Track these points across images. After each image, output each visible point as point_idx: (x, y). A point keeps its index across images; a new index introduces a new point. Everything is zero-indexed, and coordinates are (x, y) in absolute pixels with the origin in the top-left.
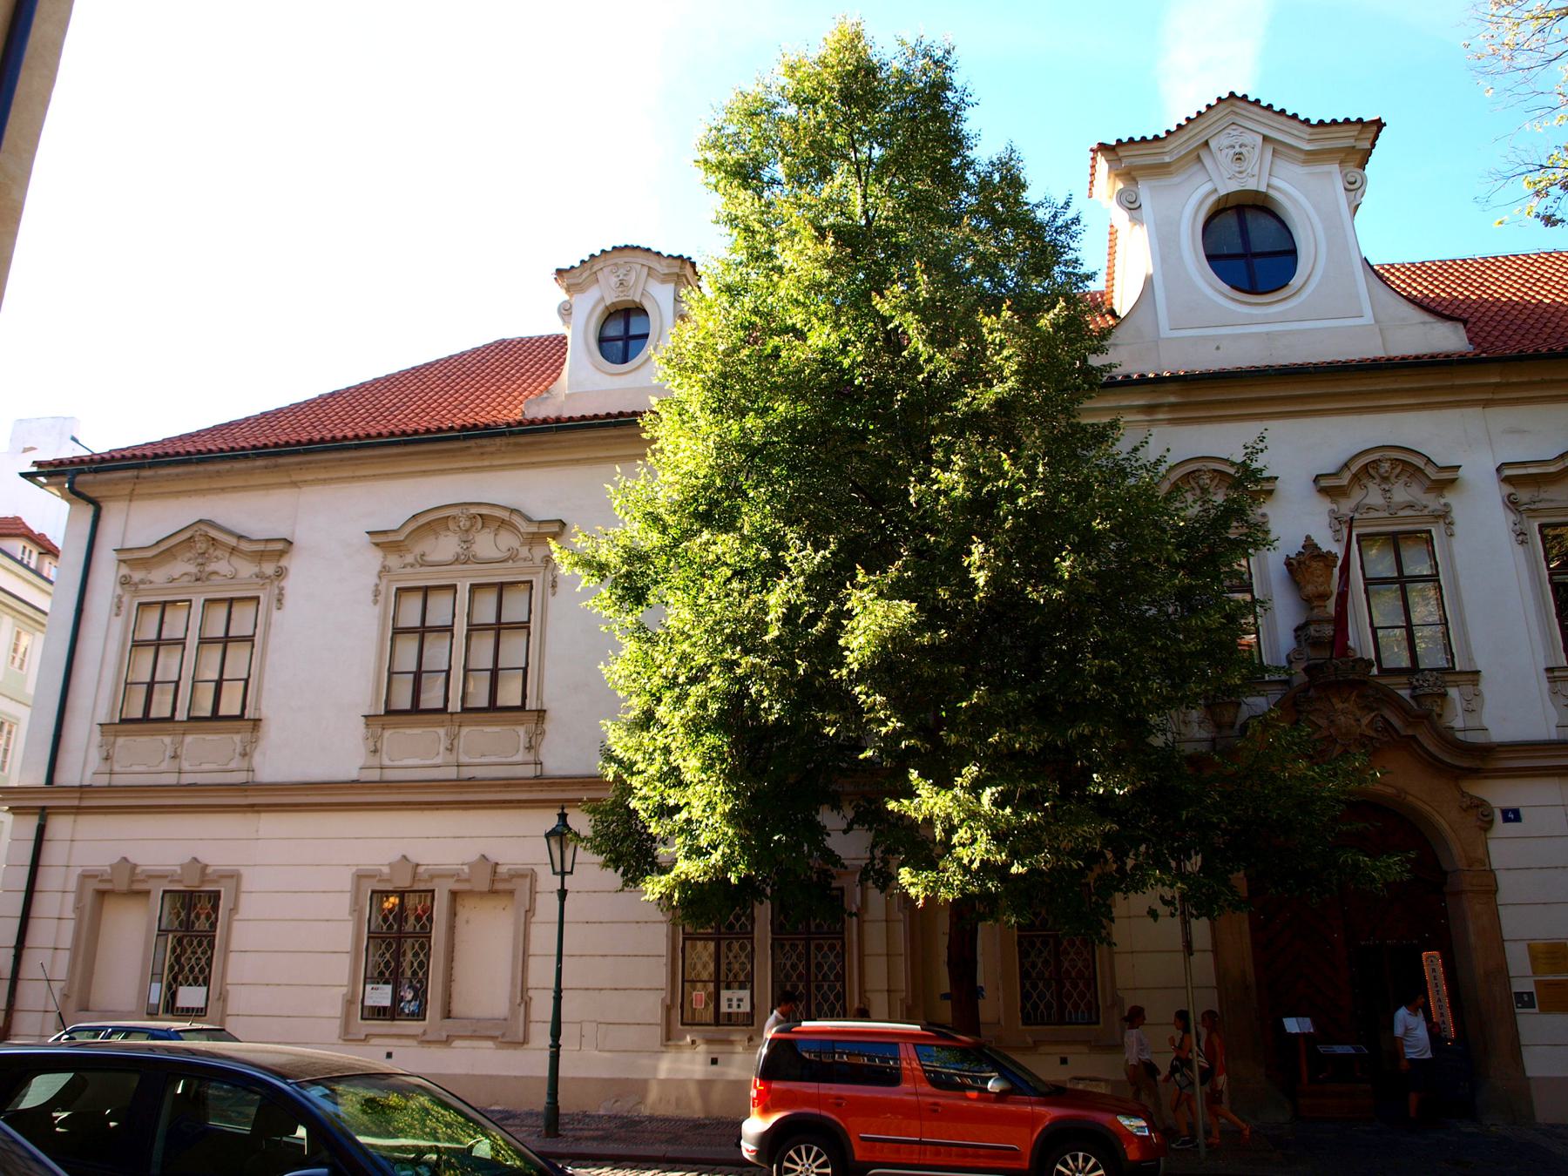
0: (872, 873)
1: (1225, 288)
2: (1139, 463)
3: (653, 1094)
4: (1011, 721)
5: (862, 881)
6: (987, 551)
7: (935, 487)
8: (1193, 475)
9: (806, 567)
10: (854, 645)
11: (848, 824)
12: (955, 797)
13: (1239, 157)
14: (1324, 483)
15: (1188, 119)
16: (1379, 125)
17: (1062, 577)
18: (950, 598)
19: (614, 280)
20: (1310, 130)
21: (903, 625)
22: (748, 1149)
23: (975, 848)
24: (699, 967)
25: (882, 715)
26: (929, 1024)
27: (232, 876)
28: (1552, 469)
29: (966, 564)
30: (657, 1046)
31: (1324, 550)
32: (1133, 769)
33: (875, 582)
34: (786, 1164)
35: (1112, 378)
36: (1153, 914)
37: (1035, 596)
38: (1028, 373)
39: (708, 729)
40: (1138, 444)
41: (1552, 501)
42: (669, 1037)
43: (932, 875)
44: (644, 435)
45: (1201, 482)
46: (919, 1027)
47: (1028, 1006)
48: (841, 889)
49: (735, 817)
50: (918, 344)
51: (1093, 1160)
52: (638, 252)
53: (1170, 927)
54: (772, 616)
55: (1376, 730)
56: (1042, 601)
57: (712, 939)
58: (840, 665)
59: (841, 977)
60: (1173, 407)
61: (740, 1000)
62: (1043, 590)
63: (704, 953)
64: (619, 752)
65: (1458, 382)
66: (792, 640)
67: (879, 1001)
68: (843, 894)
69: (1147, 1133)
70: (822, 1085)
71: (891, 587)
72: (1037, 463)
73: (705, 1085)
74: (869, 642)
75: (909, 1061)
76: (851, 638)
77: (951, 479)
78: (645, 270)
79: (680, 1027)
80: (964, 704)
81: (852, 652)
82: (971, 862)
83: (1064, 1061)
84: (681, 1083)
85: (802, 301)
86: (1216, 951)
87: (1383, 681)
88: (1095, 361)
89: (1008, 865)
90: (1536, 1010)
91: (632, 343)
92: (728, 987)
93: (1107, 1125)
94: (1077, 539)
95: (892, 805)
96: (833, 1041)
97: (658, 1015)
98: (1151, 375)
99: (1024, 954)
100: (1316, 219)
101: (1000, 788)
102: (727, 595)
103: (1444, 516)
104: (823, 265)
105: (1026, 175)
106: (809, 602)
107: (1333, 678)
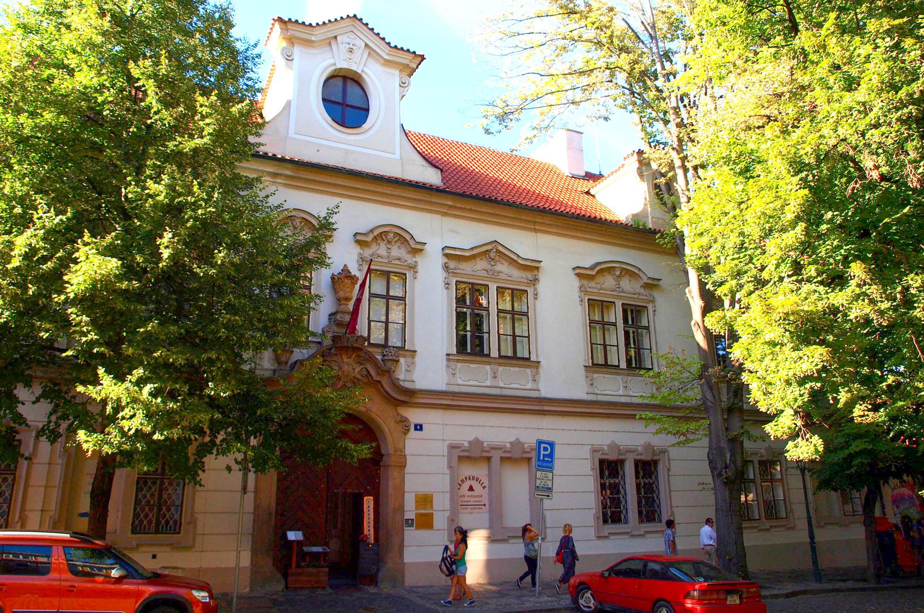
0: (47, 432)
1: (329, 119)
2: (267, 205)
4: (171, 343)
5: (37, 437)
6: (173, 238)
7: (147, 191)
9: (47, 224)
10: (73, 281)
11: (37, 398)
13: (351, 51)
14: (359, 238)
16: (423, 58)
17: (216, 262)
20: (390, 49)
21: (110, 274)
25: (85, 329)
26: (74, 533)
28: (467, 254)
29: (158, 243)
31: (353, 274)
32: (233, 382)
33: (95, 243)
35: (257, 152)
36: (229, 469)
37: (198, 270)
38: (218, 136)
40: (269, 194)
41: (463, 270)
43: (100, 437)
45: (294, 223)
46: (69, 535)
47: (137, 522)
48: (20, 441)
50: (152, 101)
53: (237, 475)
54: (16, 252)
55: (362, 376)
56: (202, 274)
58: (60, 292)
60: (287, 176)
62: (204, 268)
65: (434, 200)
66: (28, 271)
67: (34, 517)
69: (208, 600)
71: (106, 248)
72: (213, 191)
74: (85, 281)
75: (58, 557)
76: (74, 276)
77: (158, 190)
80: (142, 330)
81: (72, 285)
82: (130, 429)
83: (154, 557)
85: (79, 51)
86: (256, 492)
87: (370, 349)
88: (252, 139)
90: (414, 528)
93: (185, 596)
94: (229, 241)
95: (80, 388)
98: (279, 156)
99: (139, 489)
100: (382, 97)
101: (156, 385)
103: (413, 267)
104: (99, 33)
105: (235, 20)
106: (44, 248)
107: (346, 344)
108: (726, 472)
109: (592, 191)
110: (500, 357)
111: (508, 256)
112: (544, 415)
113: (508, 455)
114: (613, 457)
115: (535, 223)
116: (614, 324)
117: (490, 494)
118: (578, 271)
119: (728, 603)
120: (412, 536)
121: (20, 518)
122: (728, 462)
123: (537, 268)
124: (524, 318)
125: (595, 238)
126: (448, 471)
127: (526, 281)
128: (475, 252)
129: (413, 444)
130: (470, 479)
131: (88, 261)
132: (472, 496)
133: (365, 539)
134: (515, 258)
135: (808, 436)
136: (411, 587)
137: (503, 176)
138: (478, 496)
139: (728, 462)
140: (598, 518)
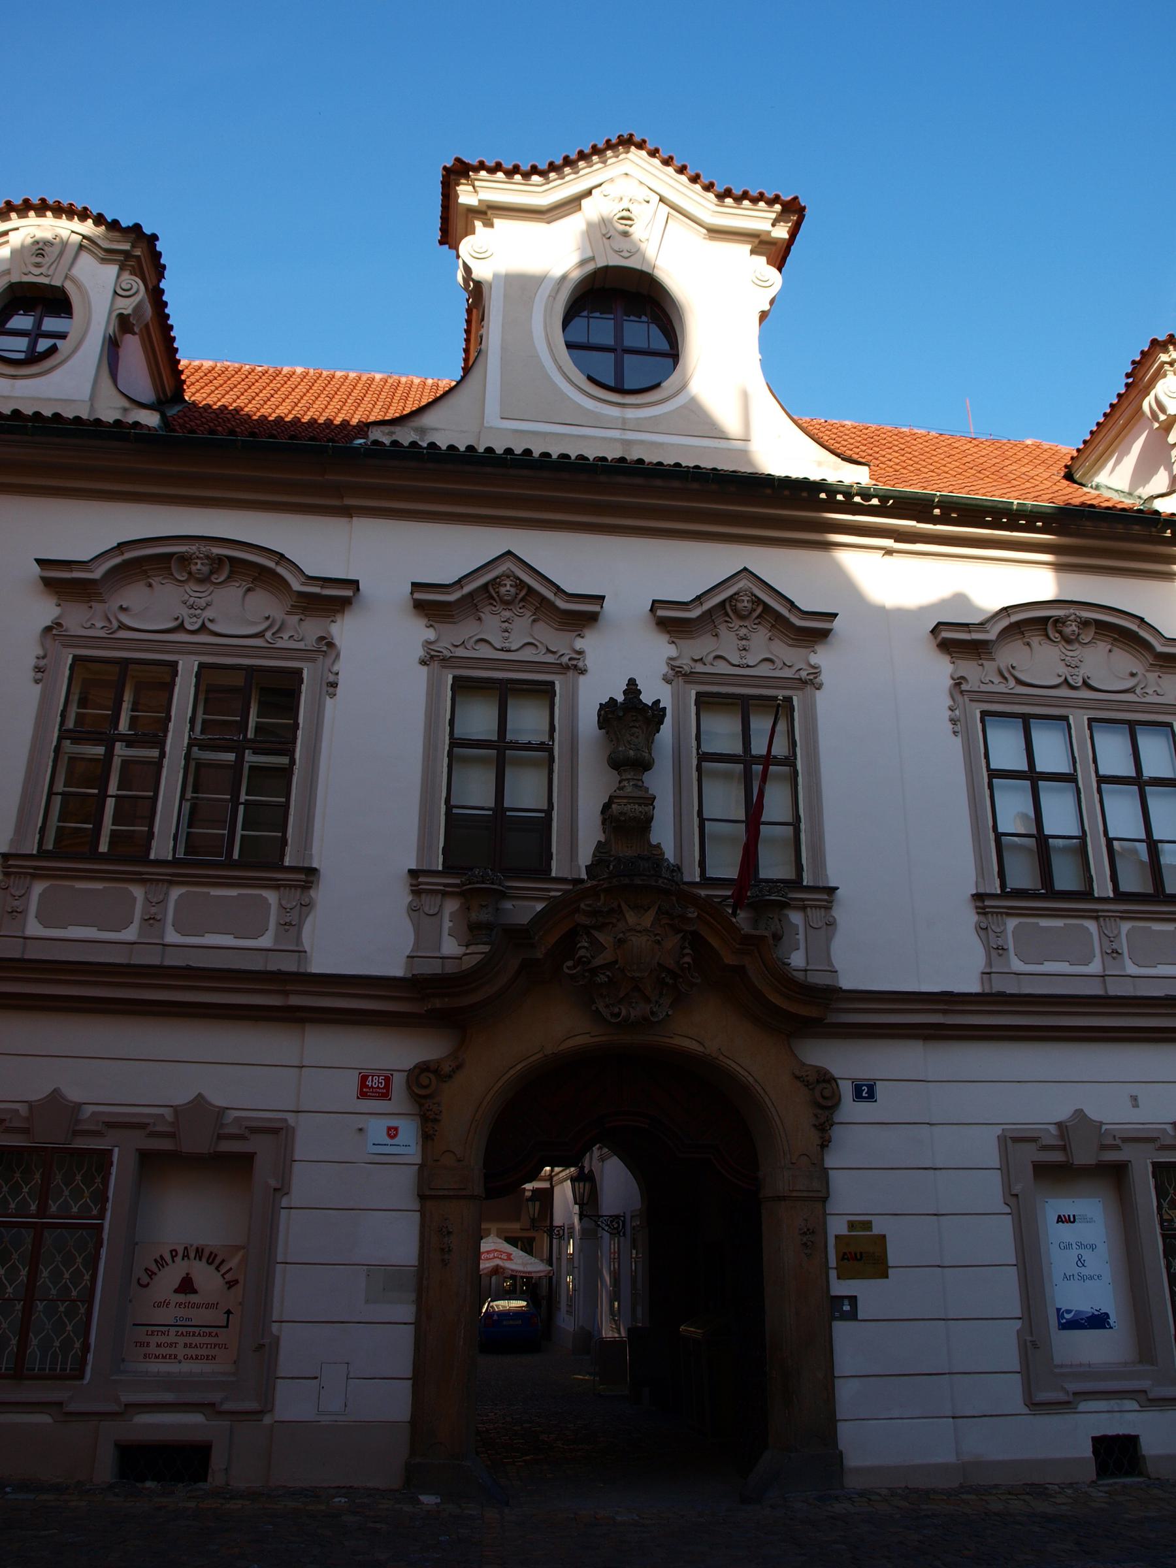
27: (275, 1131)
28: (561, 604)
103: (810, 682)
130: (186, 1256)
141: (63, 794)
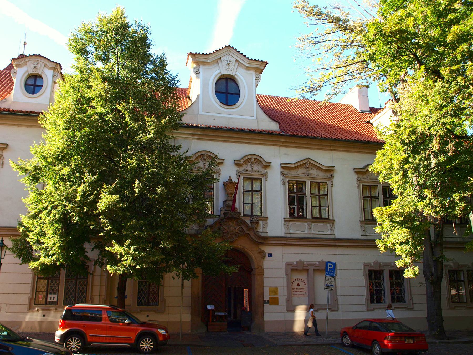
1: (219, 102)
3: (24, 325)
4: (141, 230)
5: (95, 264)
6: (139, 183)
7: (128, 163)
8: (202, 155)
9: (89, 180)
12: (124, 249)
13: (228, 64)
14: (236, 162)
15: (216, 50)
16: (266, 63)
17: (158, 192)
18: (128, 194)
19: (32, 66)
20: (248, 61)
22: (57, 339)
23: (128, 262)
24: (41, 288)
25: (106, 225)
28: (293, 166)
30: (26, 311)
34: (68, 343)
38: (157, 133)
39: (56, 222)
41: (292, 174)
42: (30, 308)
44: (39, 122)
46: (108, 306)
48: (88, 266)
49: (61, 247)
51: (151, 340)
52: (42, 58)
53: (178, 281)
54: (78, 194)
57: (46, 279)
59: (86, 291)
60: (199, 135)
61: (54, 297)
63: (43, 282)
64: (24, 223)
67: (96, 298)
68: (88, 267)
70: (80, 321)
73: (41, 323)
75: (105, 315)
77: (133, 162)
78: (44, 65)
79: (34, 305)
80: (129, 224)
82: (126, 265)
83: (148, 316)
84: (33, 322)
89: (136, 266)
91: (37, 88)
92: (51, 293)
96: (84, 310)
97: (27, 301)
99: (139, 286)
100: (246, 86)
101: (136, 246)
102: (66, 186)
103: (265, 175)
107: (230, 217)
108: (431, 277)
109: (371, 121)
110: (313, 218)
111: (315, 165)
112: (337, 247)
113: (318, 268)
114: (377, 268)
115: (331, 146)
116: (378, 198)
117: (308, 288)
118: (355, 170)
119: (406, 342)
120: (267, 308)
121: (91, 298)
122: (433, 272)
123: (333, 170)
124: (326, 197)
125: (366, 151)
126: (286, 277)
127: (326, 177)
128: (297, 165)
129: (267, 263)
130: (298, 280)
131: (105, 198)
132: (299, 289)
133: (244, 309)
134: (320, 166)
135: (413, 267)
136: (268, 332)
137: (318, 118)
138: (302, 289)
139: (433, 272)
140: (368, 300)
141: (304, 206)
